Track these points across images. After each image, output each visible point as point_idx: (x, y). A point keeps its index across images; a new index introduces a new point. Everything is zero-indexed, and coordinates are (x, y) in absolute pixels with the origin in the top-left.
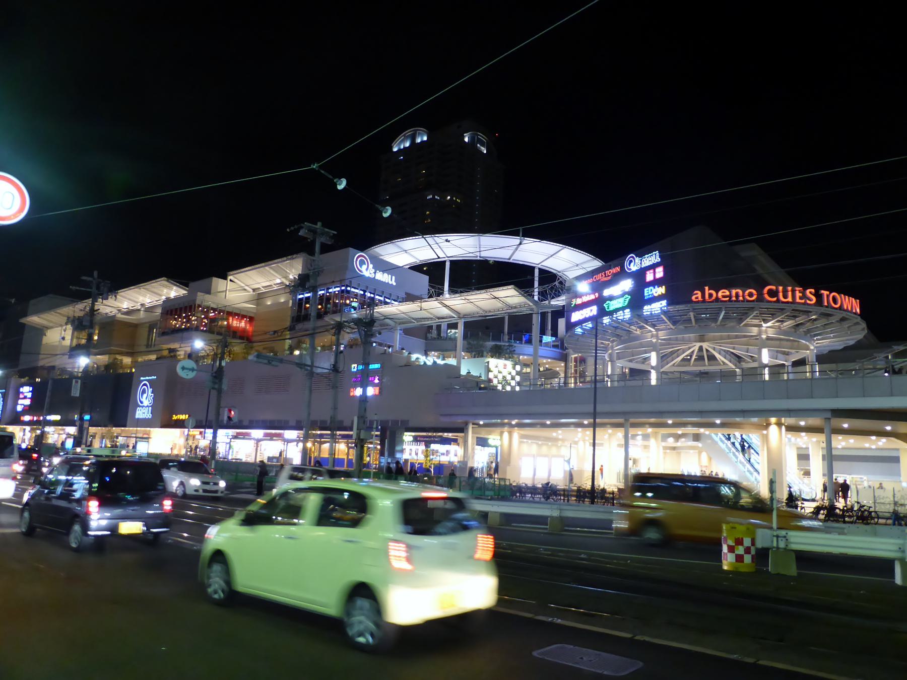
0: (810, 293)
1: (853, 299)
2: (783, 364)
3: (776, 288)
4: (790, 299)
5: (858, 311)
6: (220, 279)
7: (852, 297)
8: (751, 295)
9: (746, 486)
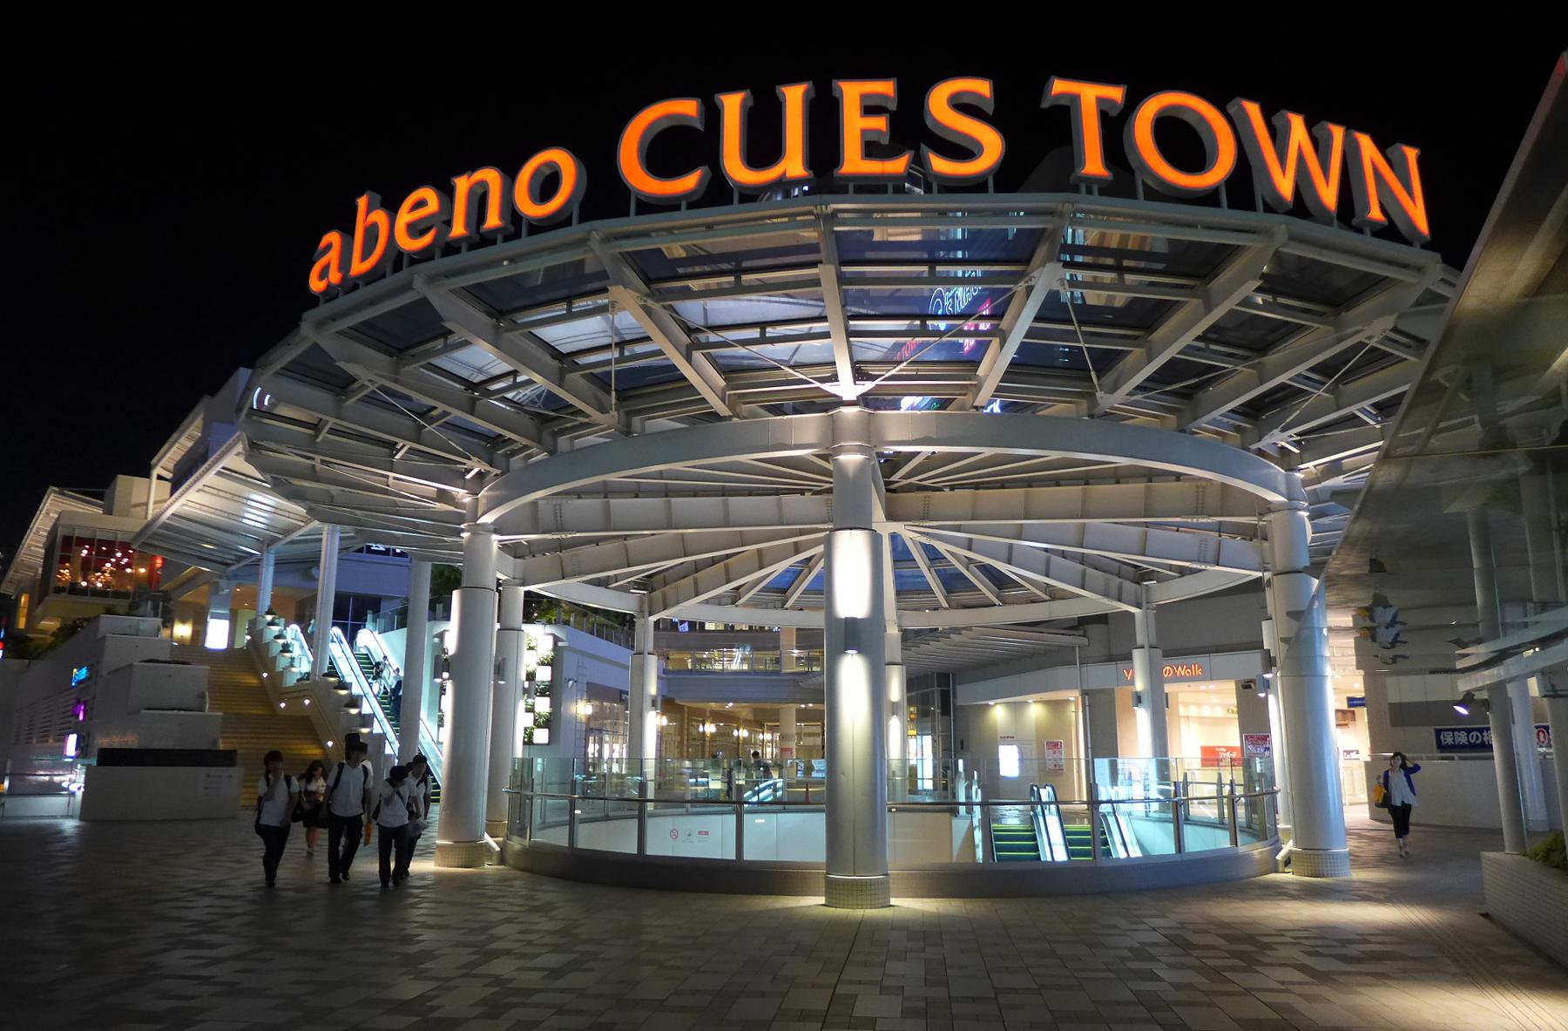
0: (963, 106)
1: (1366, 143)
2: (1127, 612)
3: (1276, 300)
4: (793, 164)
5: (1418, 215)
6: (136, 479)
7: (1353, 123)
8: (547, 185)
9: (1376, 985)
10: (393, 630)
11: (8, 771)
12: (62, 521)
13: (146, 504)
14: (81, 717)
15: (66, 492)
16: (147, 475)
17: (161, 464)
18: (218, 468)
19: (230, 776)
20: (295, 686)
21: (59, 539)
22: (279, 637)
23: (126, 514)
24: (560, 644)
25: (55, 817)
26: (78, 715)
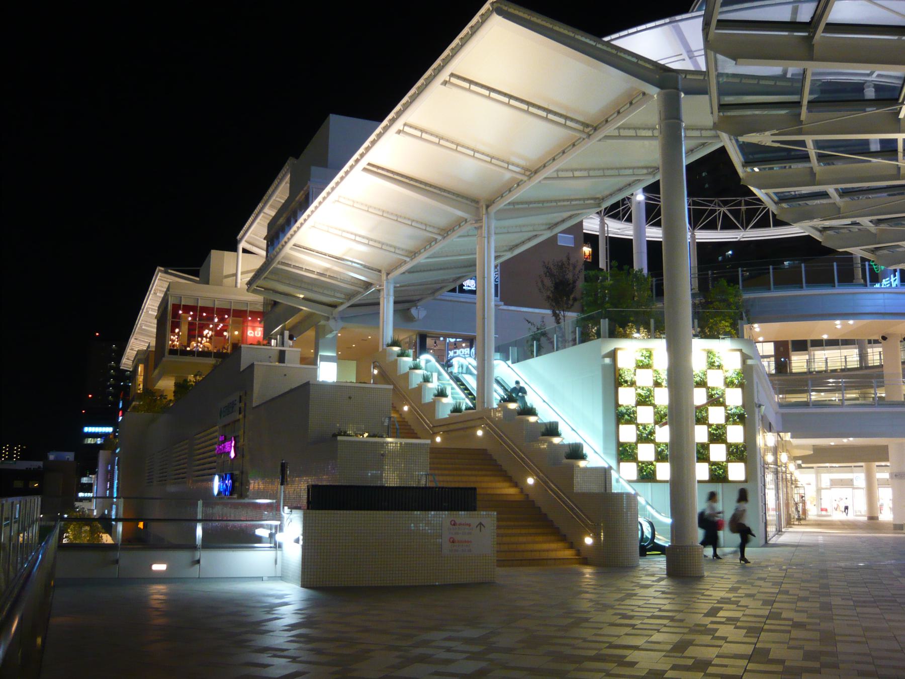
6: (226, 253)
10: (532, 356)
11: (199, 517)
12: (171, 291)
13: (236, 275)
14: (232, 455)
15: (169, 271)
16: (234, 249)
17: (246, 238)
18: (363, 163)
19: (481, 524)
20: (450, 418)
21: (170, 307)
22: (416, 367)
23: (220, 284)
24: (749, 362)
25: (261, 579)
26: (229, 452)
